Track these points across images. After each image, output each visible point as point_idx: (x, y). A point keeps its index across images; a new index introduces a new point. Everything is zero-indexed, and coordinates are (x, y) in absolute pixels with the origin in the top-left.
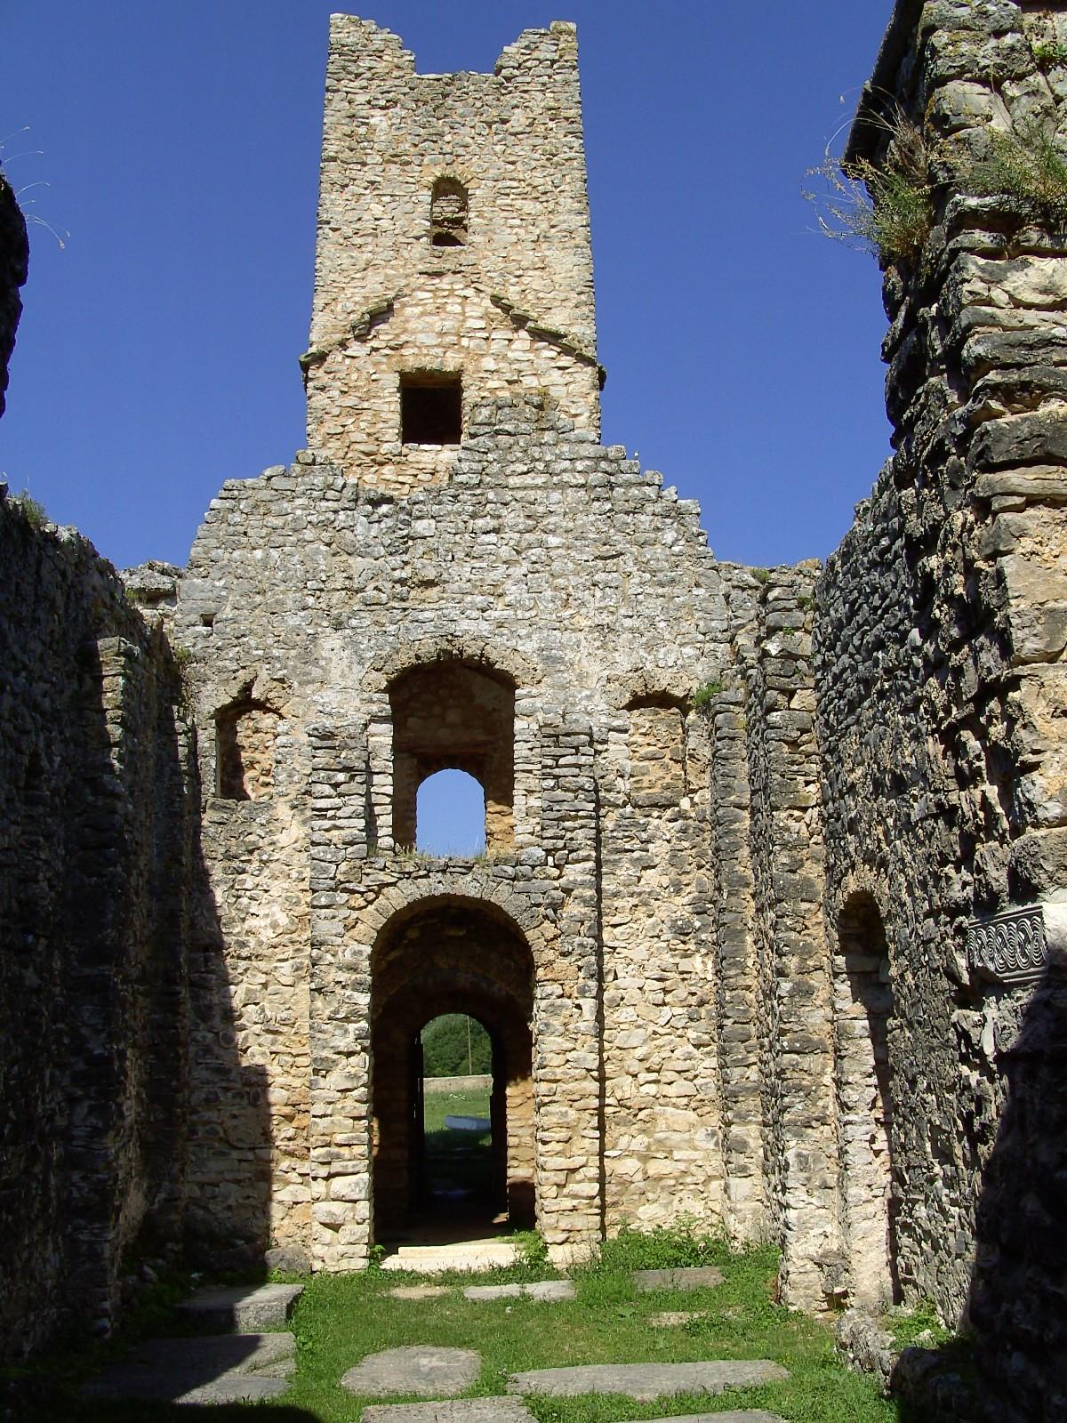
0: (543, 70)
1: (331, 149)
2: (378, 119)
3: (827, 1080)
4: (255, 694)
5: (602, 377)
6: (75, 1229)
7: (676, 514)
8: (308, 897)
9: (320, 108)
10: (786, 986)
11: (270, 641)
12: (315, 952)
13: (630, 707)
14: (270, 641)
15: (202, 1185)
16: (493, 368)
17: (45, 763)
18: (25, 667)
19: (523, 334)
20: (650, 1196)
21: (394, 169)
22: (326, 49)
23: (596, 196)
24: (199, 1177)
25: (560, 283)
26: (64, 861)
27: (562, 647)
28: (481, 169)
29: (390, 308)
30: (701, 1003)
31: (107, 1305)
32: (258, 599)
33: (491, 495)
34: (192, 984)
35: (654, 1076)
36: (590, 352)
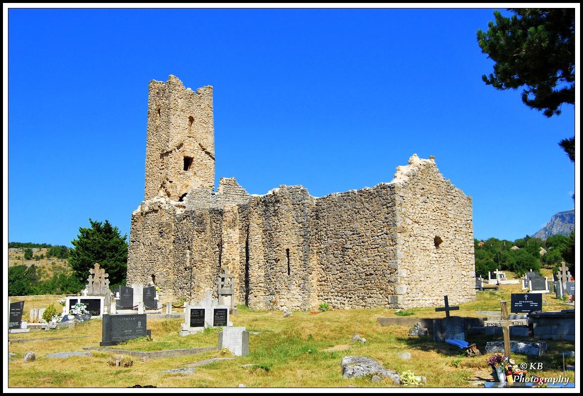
0: (206, 91)
23: (216, 126)
25: (209, 141)
28: (196, 115)
36: (214, 157)
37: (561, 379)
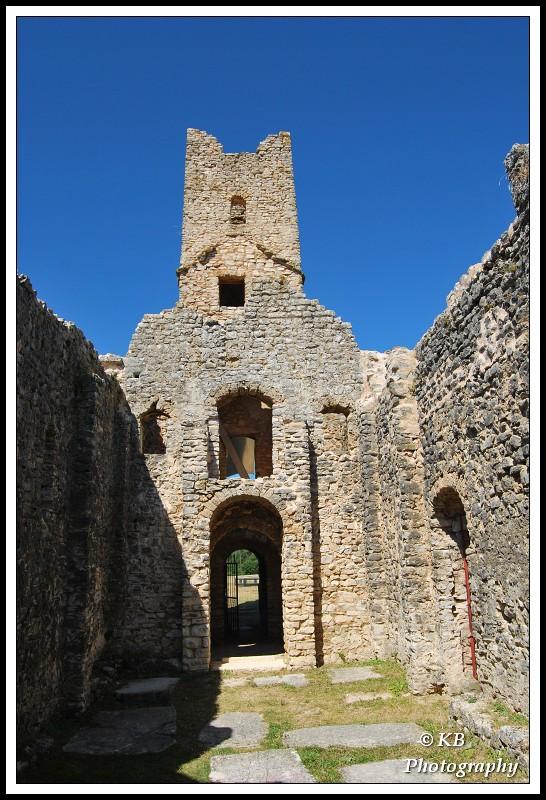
0: (276, 153)
1: (188, 184)
2: (207, 171)
3: (428, 578)
4: (158, 407)
5: (303, 279)
6: (69, 657)
7: (340, 329)
8: (182, 497)
9: (183, 167)
10: (407, 534)
11: (165, 384)
12: (185, 522)
13: (324, 412)
14: (165, 384)
15: (132, 631)
16: (256, 273)
17: (56, 429)
18: (46, 382)
19: (270, 260)
20: (337, 632)
21: (214, 193)
22: (184, 143)
23: (301, 205)
24: (130, 627)
25: (285, 238)
26: (66, 478)
27: (293, 386)
28: (253, 191)
29: (214, 250)
30: (358, 544)
31: (83, 695)
32: (160, 366)
33: (261, 321)
34: (129, 537)
35: (337, 577)
36: (298, 268)
37: (502, 767)
